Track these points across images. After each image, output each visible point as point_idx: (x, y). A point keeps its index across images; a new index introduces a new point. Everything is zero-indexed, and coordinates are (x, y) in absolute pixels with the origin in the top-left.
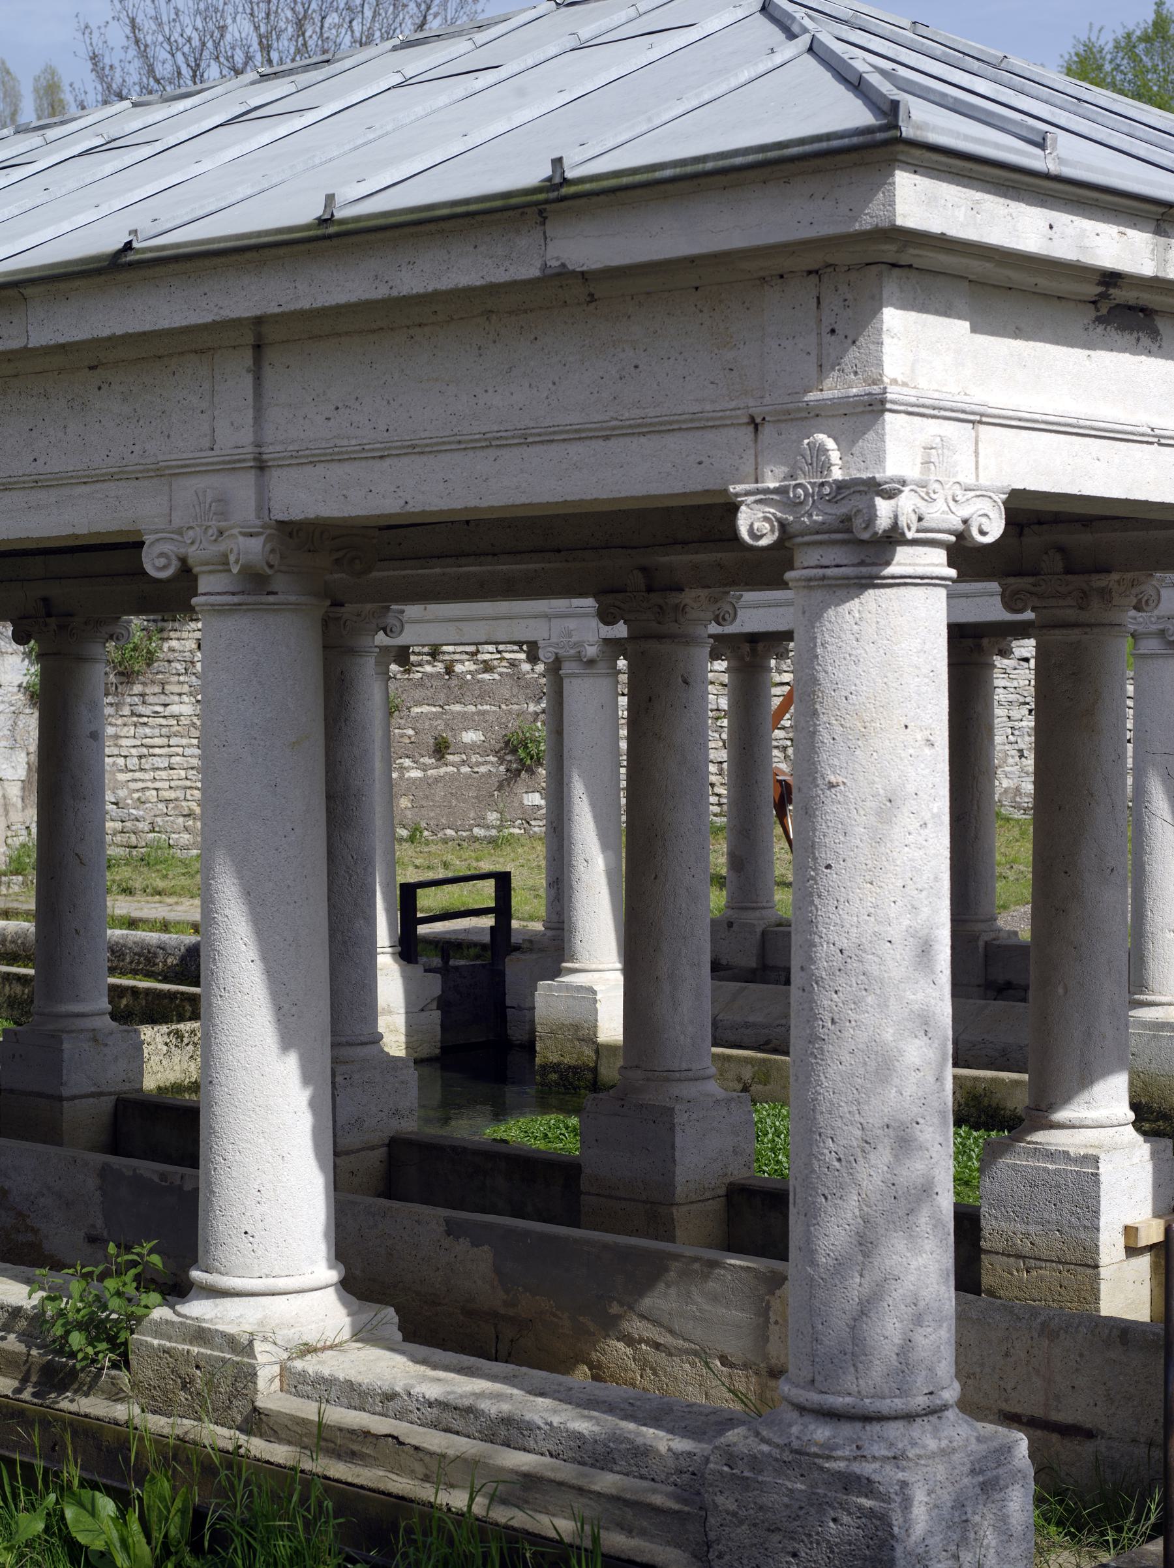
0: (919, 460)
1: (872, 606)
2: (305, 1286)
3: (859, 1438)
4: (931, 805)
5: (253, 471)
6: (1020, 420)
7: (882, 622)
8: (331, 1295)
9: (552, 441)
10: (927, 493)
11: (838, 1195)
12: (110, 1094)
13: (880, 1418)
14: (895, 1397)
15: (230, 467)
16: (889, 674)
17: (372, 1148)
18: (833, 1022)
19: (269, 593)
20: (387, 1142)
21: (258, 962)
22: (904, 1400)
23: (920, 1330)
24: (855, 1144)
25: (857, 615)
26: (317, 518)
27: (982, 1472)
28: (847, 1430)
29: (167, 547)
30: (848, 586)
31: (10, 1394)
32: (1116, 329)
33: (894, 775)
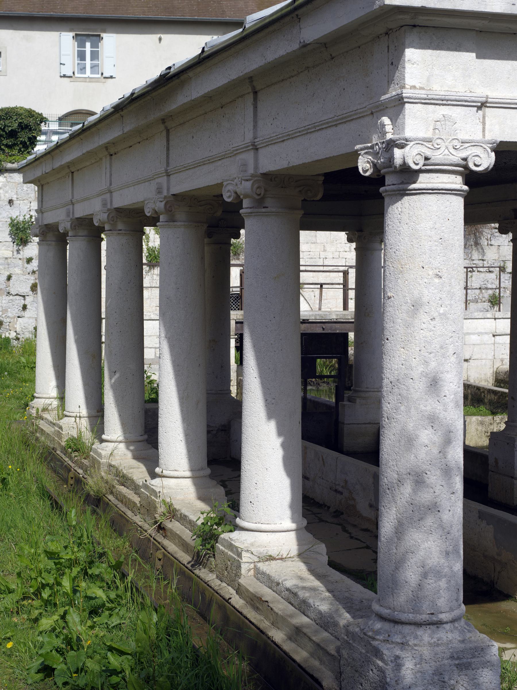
0: (432, 128)
1: (407, 205)
2: (275, 529)
3: (391, 631)
4: (438, 309)
5: (253, 150)
7: (411, 213)
8: (293, 535)
9: (323, 129)
10: (433, 145)
11: (388, 507)
13: (402, 623)
14: (410, 613)
15: (245, 150)
16: (414, 240)
18: (388, 419)
19: (264, 207)
21: (258, 378)
22: (414, 615)
23: (426, 581)
24: (395, 481)
25: (400, 210)
26: (269, 171)
27: (458, 658)
28: (387, 626)
29: (230, 188)
30: (396, 195)
31: (186, 564)
33: (416, 293)
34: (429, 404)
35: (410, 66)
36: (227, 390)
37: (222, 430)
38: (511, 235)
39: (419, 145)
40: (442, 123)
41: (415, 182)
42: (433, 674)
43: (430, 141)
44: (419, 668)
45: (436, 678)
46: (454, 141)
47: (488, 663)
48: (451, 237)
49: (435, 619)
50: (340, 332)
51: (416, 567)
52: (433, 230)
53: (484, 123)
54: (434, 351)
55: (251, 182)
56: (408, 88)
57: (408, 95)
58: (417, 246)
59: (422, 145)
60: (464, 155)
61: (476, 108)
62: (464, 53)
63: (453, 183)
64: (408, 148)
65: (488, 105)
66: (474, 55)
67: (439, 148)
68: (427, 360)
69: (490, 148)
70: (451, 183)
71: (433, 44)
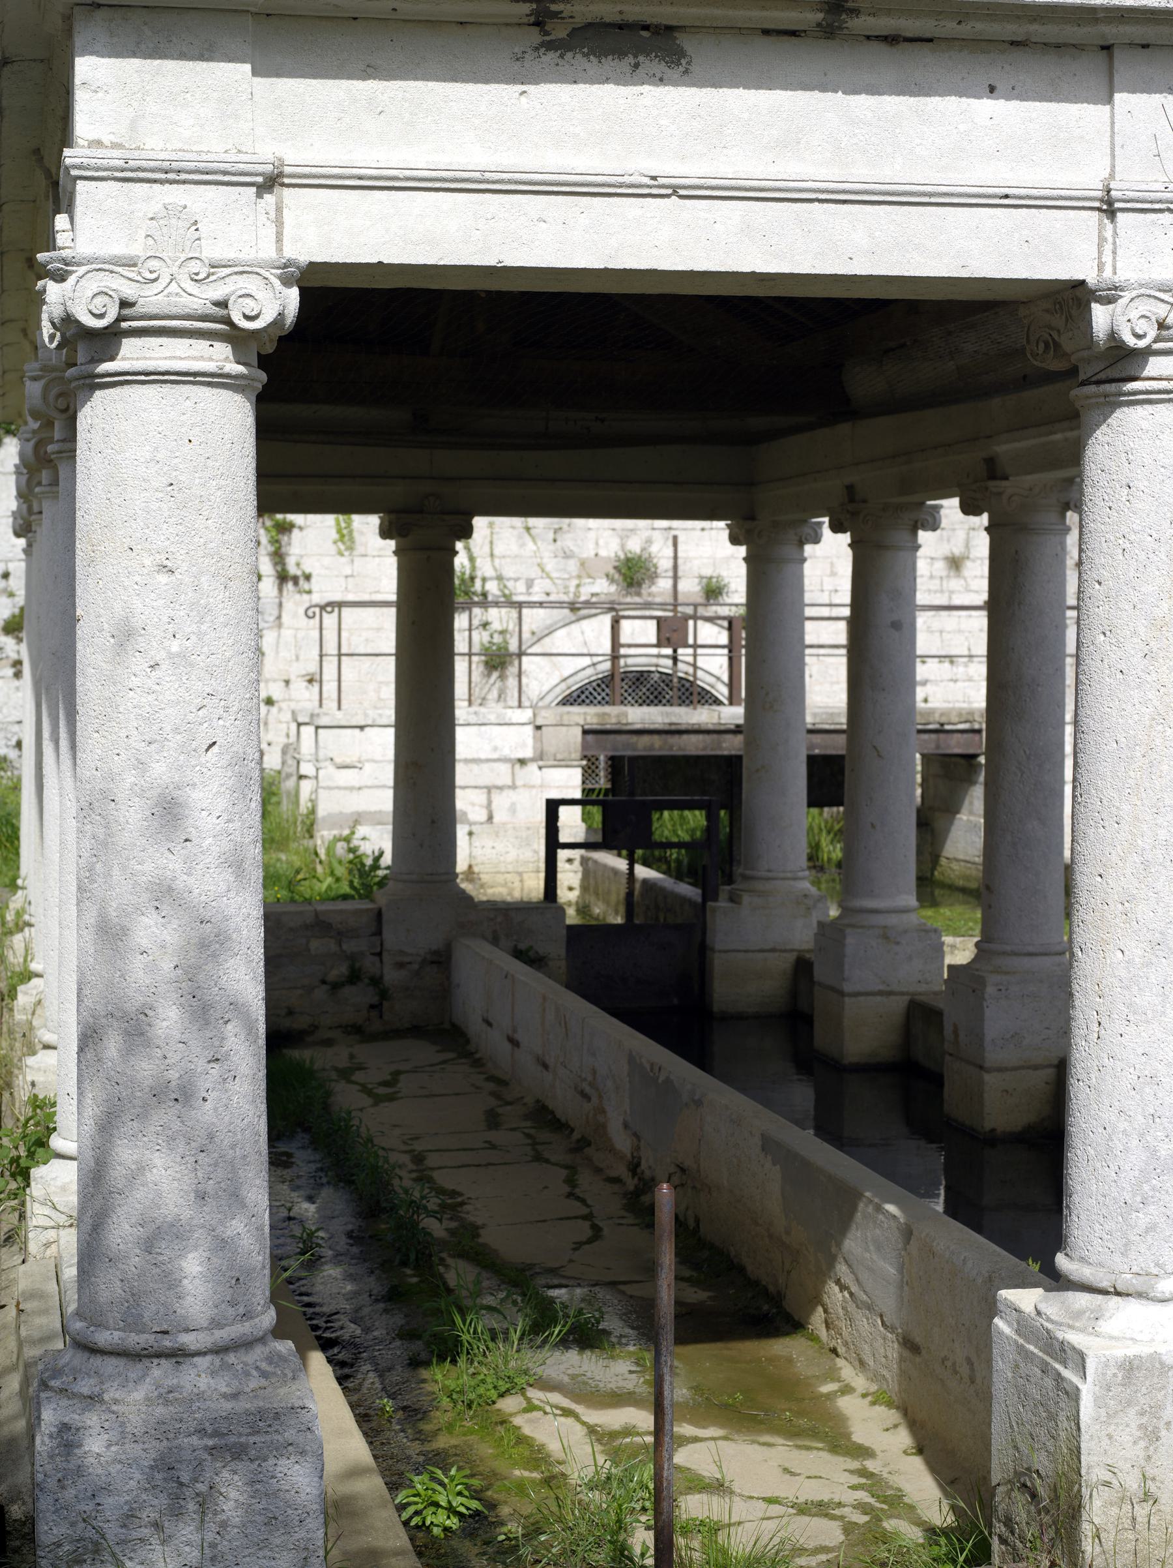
4: (167, 643)
6: (360, 178)
12: (902, 994)
14: (118, 1329)
17: (1036, 1068)
20: (1056, 1062)
27: (216, 1434)
32: (586, 55)
34: (150, 857)
35: (87, 97)
36: (447, 873)
37: (433, 962)
38: (985, 516)
39: (102, 274)
40: (162, 222)
41: (112, 359)
42: (151, 1467)
43: (131, 263)
44: (117, 1453)
45: (159, 1476)
46: (193, 262)
47: (290, 1448)
48: (197, 481)
49: (167, 1343)
50: (823, 752)
51: (127, 1227)
52: (152, 464)
53: (279, 222)
54: (158, 738)
55: (43, 382)
56: (83, 147)
57: (77, 161)
58: (118, 501)
59: (112, 272)
60: (218, 293)
61: (254, 189)
62: (222, 64)
63: (202, 358)
64: (72, 280)
65: (286, 181)
66: (247, 67)
67: (156, 280)
68: (142, 758)
69: (280, 277)
70: (195, 358)
71: (143, 46)
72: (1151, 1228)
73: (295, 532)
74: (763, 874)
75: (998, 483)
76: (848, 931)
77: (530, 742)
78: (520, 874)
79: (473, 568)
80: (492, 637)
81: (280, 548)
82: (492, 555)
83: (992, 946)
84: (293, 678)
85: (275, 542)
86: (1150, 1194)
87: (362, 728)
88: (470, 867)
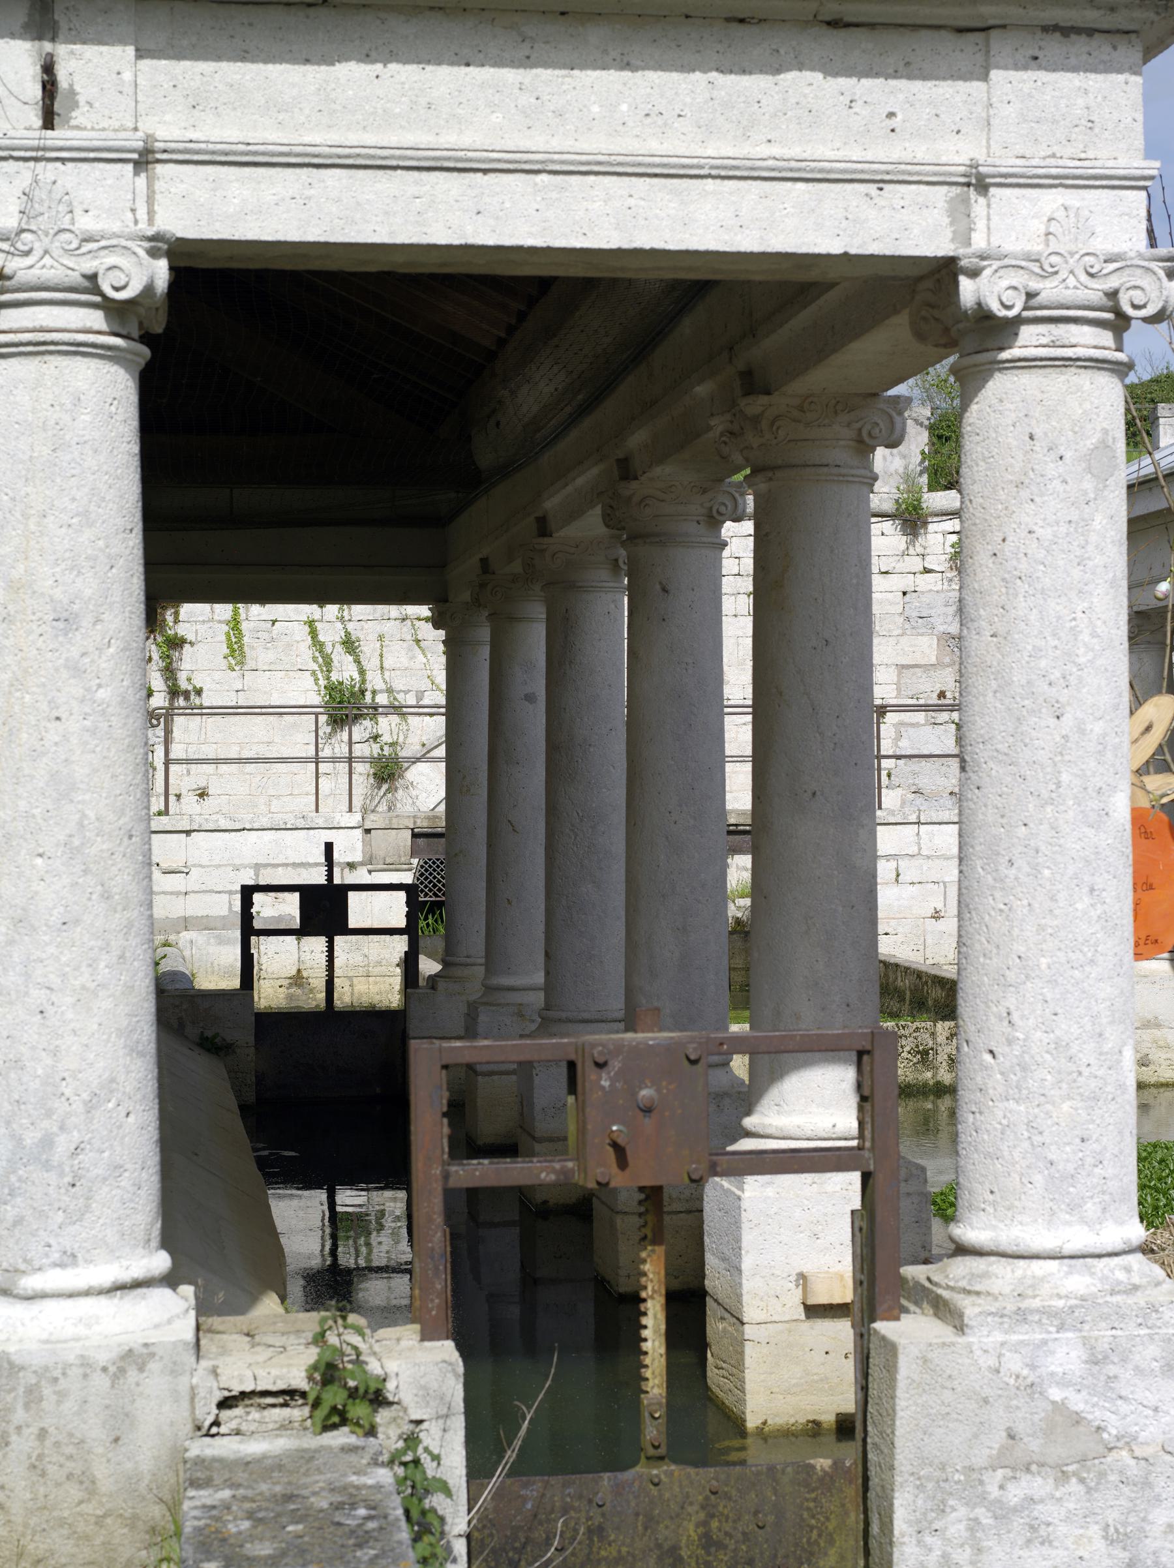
72: (19, 1221)
73: (187, 646)
74: (463, 960)
75: (546, 539)
76: (481, 1008)
77: (359, 845)
78: (350, 978)
79: (363, 681)
80: (382, 750)
81: (170, 663)
82: (382, 668)
83: (551, 1014)
84: (184, 792)
85: (166, 657)
86: (17, 1185)
87: (188, 833)
88: (299, 971)
